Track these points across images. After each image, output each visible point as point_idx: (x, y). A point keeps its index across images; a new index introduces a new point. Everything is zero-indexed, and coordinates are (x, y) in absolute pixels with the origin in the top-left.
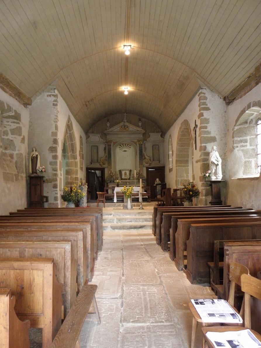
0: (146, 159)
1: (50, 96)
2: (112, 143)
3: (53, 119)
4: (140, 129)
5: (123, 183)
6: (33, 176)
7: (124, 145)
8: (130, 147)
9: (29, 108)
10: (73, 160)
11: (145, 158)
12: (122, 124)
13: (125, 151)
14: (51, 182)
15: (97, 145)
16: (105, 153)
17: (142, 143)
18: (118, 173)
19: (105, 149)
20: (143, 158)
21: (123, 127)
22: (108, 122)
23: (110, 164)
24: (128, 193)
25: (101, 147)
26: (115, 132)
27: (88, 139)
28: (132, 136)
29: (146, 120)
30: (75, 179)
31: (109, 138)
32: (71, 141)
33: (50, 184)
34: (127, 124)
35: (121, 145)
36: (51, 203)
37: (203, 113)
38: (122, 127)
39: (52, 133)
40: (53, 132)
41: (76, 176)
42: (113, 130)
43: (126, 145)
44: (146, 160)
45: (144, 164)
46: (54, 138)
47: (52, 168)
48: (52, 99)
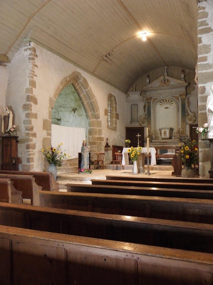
0: (190, 115)
1: (26, 50)
2: (152, 100)
3: (28, 74)
4: (181, 82)
5: (160, 143)
6: (5, 136)
7: (167, 102)
8: (171, 103)
9: (9, 66)
10: (95, 120)
11: (188, 115)
12: (162, 78)
13: (167, 108)
14: (24, 143)
15: (136, 103)
16: (145, 111)
17: (184, 98)
18: (159, 132)
19: (145, 107)
20: (186, 114)
21: (163, 81)
22: (148, 78)
23: (149, 122)
24: (132, 154)
25: (141, 105)
26: (153, 88)
27: (128, 98)
28: (174, 90)
29: (190, 70)
30: (98, 139)
31: (148, 94)
32: (89, 100)
33: (23, 144)
34: (167, 77)
35: (161, 101)
36: (24, 165)
37: (201, 37)
38: (161, 82)
39: (26, 89)
40: (27, 88)
41: (98, 136)
42: (153, 86)
43: (167, 102)
44: (190, 117)
45: (187, 120)
46: (27, 95)
47: (25, 127)
48: (28, 54)
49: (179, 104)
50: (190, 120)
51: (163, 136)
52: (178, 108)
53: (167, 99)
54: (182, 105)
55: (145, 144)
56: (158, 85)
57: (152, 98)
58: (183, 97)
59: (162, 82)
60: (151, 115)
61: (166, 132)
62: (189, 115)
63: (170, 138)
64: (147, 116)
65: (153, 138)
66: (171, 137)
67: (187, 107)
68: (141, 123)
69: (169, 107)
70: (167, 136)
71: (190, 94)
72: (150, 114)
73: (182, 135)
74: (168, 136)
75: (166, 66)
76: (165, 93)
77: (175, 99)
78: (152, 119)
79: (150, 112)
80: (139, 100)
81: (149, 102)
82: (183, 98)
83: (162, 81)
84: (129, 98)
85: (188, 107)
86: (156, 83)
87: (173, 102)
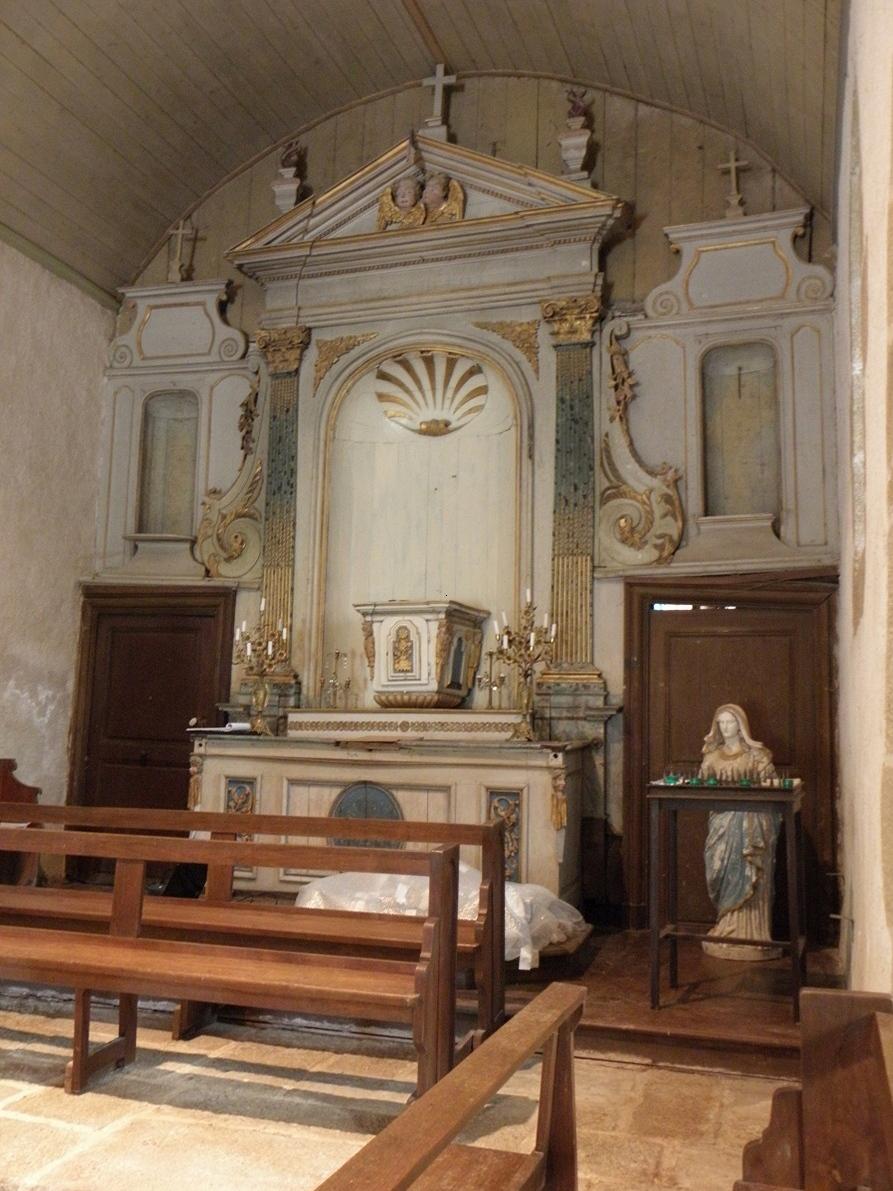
2: (312, 354)
11: (617, 490)
13: (437, 429)
15: (186, 382)
17: (586, 337)
20: (601, 483)
21: (406, 195)
23: (279, 548)
25: (225, 396)
27: (120, 340)
28: (497, 272)
31: (282, 306)
34: (441, 158)
44: (628, 506)
49: (535, 387)
50: (631, 537)
51: (381, 678)
52: (531, 426)
53: (436, 343)
54: (561, 400)
55: (197, 750)
56: (368, 220)
57: (316, 336)
58: (573, 331)
59: (399, 200)
60: (292, 486)
61: (413, 637)
62: (622, 495)
63: (454, 697)
64: (263, 496)
65: (299, 693)
66: (455, 684)
67: (606, 416)
68: (212, 550)
69: (453, 425)
70: (424, 676)
71: (634, 313)
72: (293, 472)
73: (551, 679)
74: (426, 676)
75: (440, 69)
76: (421, 294)
77: (508, 345)
78: (300, 522)
79: (294, 458)
80: (209, 353)
81: (289, 373)
82: (575, 339)
83: (399, 192)
84: (128, 339)
85: (612, 419)
86: (352, 208)
87: (489, 378)
